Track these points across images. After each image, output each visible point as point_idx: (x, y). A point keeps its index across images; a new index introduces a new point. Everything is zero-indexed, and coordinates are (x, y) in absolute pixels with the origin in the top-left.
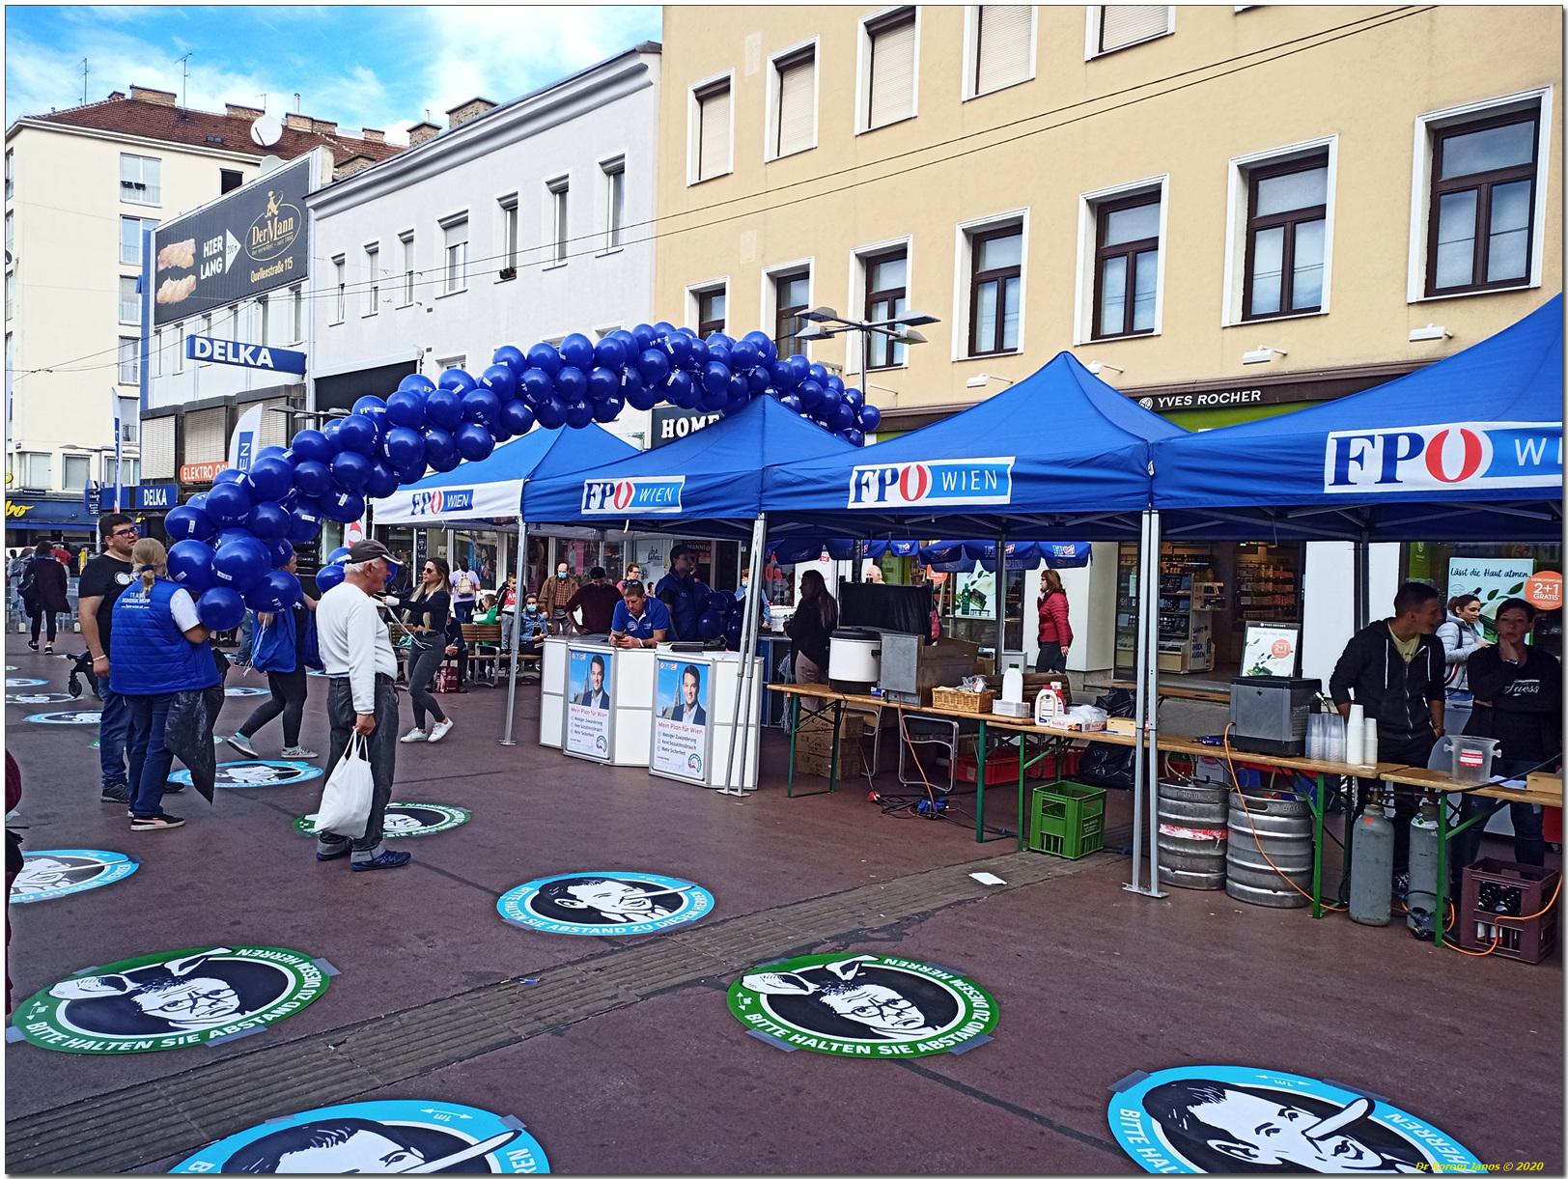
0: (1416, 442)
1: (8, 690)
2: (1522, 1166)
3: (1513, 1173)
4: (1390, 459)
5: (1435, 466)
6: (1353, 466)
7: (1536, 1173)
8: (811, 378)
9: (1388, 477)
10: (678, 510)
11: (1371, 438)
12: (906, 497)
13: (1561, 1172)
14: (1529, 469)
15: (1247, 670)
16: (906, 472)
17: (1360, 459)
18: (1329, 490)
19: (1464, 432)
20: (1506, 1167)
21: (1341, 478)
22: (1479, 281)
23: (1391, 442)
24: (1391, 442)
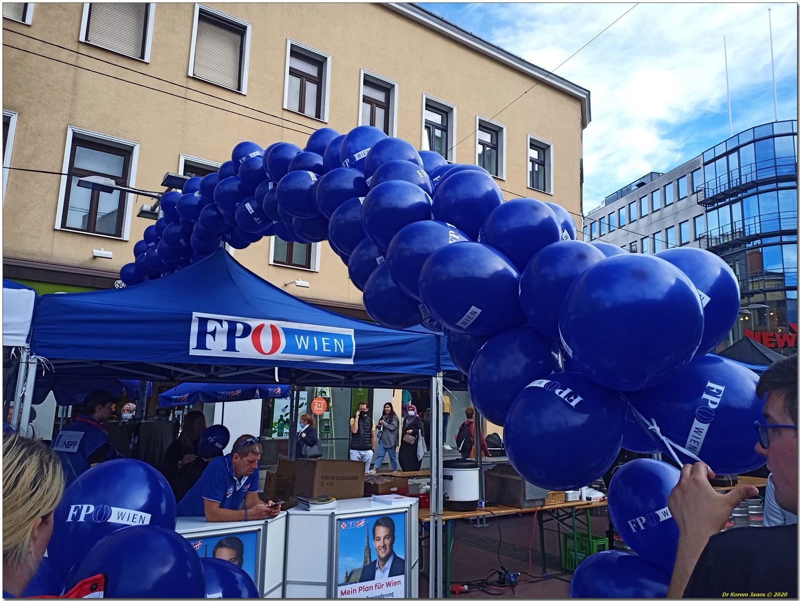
0: (247, 330)
1: (436, 597)
2: (777, 594)
3: (772, 597)
4: (231, 334)
5: (258, 346)
6: (209, 338)
7: (784, 598)
8: (301, 162)
9: (231, 347)
10: (350, 362)
11: (220, 322)
12: (260, 350)
13: (795, 596)
14: (303, 352)
15: (351, 451)
16: (260, 328)
17: (213, 333)
18: (193, 352)
19: (272, 326)
20: (768, 595)
21: (201, 345)
22: (73, 171)
23: (232, 325)
24: (232, 325)
